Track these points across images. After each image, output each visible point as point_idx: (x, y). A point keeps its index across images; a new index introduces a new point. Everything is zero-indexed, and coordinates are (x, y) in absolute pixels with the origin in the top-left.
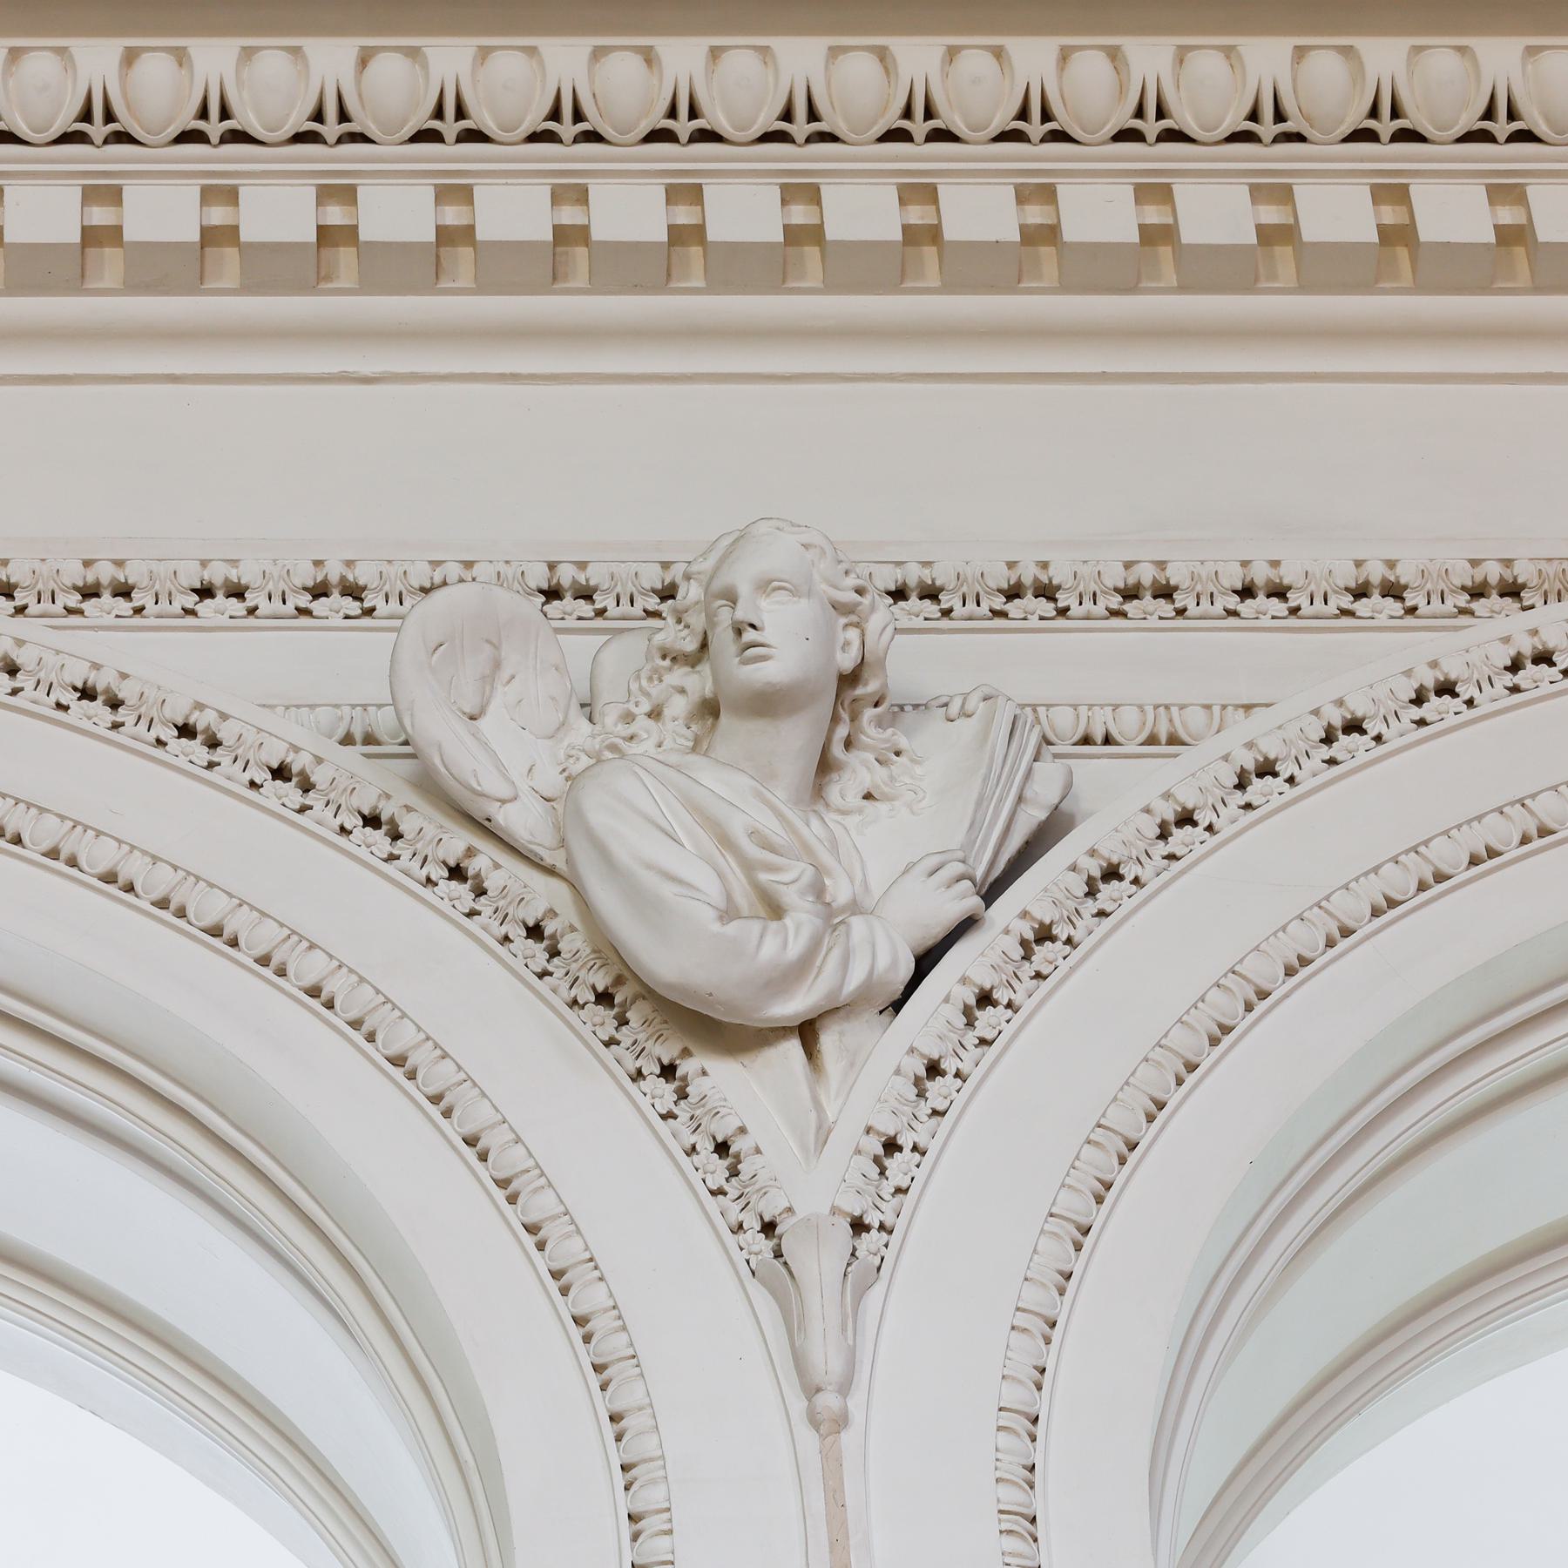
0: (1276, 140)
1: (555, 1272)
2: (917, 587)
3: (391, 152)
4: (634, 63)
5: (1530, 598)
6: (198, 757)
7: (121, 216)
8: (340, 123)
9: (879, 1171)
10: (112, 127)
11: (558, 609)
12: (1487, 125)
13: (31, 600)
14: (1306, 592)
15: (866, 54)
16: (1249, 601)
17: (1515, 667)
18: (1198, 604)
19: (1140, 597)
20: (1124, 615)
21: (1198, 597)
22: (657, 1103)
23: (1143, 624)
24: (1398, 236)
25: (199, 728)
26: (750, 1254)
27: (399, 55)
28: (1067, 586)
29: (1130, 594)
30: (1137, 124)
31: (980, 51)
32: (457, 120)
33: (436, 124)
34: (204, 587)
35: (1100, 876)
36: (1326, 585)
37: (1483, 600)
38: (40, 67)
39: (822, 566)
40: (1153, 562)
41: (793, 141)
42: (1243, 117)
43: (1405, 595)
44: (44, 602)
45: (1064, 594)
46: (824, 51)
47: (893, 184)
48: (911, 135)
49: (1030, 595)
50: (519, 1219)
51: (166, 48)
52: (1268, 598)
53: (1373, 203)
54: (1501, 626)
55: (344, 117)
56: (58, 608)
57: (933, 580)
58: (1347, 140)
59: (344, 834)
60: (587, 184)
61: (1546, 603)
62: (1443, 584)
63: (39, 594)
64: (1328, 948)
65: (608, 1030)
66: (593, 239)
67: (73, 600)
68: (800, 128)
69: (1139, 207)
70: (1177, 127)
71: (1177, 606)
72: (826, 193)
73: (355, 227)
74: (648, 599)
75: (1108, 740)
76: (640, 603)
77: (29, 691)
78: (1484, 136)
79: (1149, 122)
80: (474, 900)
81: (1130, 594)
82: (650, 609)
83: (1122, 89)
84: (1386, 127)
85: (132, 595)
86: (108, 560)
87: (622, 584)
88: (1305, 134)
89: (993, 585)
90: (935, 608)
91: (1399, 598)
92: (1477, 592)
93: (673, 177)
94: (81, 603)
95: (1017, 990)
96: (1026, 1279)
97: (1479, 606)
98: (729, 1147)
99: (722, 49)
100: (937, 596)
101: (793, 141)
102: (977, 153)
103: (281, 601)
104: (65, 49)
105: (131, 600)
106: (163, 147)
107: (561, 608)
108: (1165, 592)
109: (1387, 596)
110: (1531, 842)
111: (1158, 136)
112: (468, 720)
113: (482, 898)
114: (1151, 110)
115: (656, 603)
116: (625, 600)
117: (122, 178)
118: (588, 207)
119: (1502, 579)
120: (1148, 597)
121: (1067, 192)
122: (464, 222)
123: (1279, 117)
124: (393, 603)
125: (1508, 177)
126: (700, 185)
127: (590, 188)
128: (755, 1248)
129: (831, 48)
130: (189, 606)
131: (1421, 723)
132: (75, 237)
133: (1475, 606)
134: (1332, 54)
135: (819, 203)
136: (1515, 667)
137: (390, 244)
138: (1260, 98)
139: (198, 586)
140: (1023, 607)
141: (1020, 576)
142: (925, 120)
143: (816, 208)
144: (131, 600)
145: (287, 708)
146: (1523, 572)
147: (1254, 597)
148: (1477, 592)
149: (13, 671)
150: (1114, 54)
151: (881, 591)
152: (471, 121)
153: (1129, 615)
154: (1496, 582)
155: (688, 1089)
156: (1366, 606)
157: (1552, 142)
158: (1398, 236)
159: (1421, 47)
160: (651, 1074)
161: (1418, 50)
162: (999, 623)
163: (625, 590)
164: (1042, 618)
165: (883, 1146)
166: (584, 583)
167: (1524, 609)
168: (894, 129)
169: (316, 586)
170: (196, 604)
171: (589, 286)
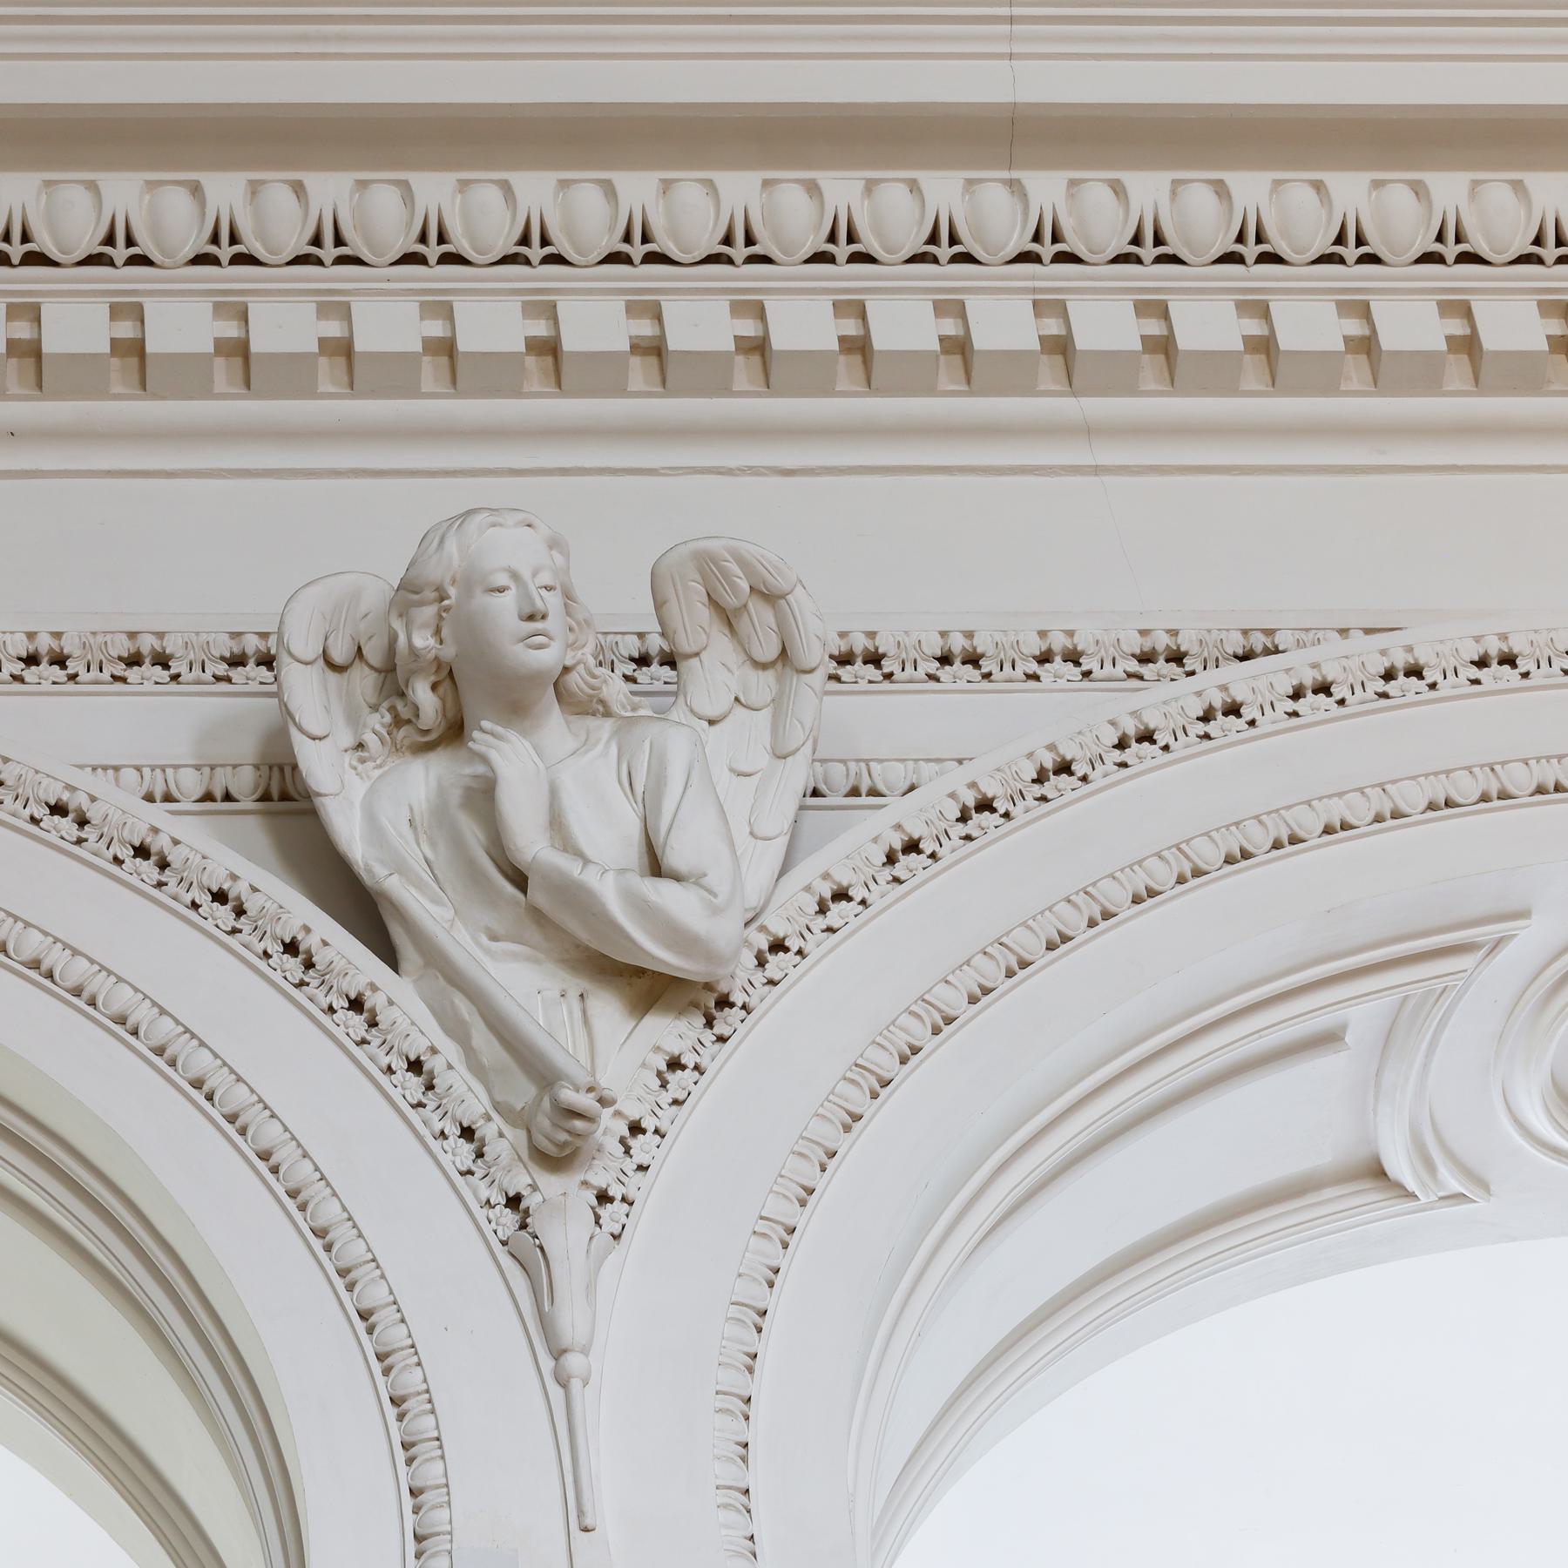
1: (342, 1270)
2: (48, 653)
5: (987, 666)
8: (335, 247)
11: (242, 674)
12: (1338, 249)
14: (1096, 658)
15: (1506, 184)
16: (947, 668)
18: (903, 670)
19: (1050, 660)
20: (229, 680)
21: (903, 663)
27: (1509, 186)
28: (1090, 652)
30: (1035, 247)
31: (1101, 183)
32: (848, 243)
33: (830, 248)
35: (830, 897)
36: (1217, 652)
39: (101, 640)
42: (1128, 241)
46: (554, 182)
50: (309, 1224)
51: (593, 180)
53: (1136, 315)
54: (1165, 690)
55: (339, 241)
56: (208, 676)
58: (807, 261)
60: (864, 300)
61: (1205, 669)
62: (1549, 650)
63: (1205, 660)
69: (1038, 320)
70: (1472, 250)
79: (942, 245)
87: (1105, 649)
88: (1380, 255)
91: (166, 667)
92: (1146, 658)
96: (740, 1275)
97: (1148, 670)
99: (263, 182)
102: (893, 273)
107: (245, 674)
109: (157, 664)
112: (727, 770)
113: (242, 919)
114: (1451, 236)
117: (750, 294)
119: (964, 648)
120: (1161, 661)
126: (451, 301)
127: (455, 305)
129: (1173, 181)
130: (629, 673)
134: (81, 188)
137: (84, 355)
138: (1544, 227)
139: (636, 655)
142: (642, 244)
145: (94, 769)
147: (38, 664)
148: (1146, 658)
150: (913, 186)
151: (626, 658)
152: (861, 245)
153: (233, 681)
161: (363, 184)
162: (119, 687)
164: (870, 682)
169: (130, 656)
170: (634, 670)
171: (1475, 389)
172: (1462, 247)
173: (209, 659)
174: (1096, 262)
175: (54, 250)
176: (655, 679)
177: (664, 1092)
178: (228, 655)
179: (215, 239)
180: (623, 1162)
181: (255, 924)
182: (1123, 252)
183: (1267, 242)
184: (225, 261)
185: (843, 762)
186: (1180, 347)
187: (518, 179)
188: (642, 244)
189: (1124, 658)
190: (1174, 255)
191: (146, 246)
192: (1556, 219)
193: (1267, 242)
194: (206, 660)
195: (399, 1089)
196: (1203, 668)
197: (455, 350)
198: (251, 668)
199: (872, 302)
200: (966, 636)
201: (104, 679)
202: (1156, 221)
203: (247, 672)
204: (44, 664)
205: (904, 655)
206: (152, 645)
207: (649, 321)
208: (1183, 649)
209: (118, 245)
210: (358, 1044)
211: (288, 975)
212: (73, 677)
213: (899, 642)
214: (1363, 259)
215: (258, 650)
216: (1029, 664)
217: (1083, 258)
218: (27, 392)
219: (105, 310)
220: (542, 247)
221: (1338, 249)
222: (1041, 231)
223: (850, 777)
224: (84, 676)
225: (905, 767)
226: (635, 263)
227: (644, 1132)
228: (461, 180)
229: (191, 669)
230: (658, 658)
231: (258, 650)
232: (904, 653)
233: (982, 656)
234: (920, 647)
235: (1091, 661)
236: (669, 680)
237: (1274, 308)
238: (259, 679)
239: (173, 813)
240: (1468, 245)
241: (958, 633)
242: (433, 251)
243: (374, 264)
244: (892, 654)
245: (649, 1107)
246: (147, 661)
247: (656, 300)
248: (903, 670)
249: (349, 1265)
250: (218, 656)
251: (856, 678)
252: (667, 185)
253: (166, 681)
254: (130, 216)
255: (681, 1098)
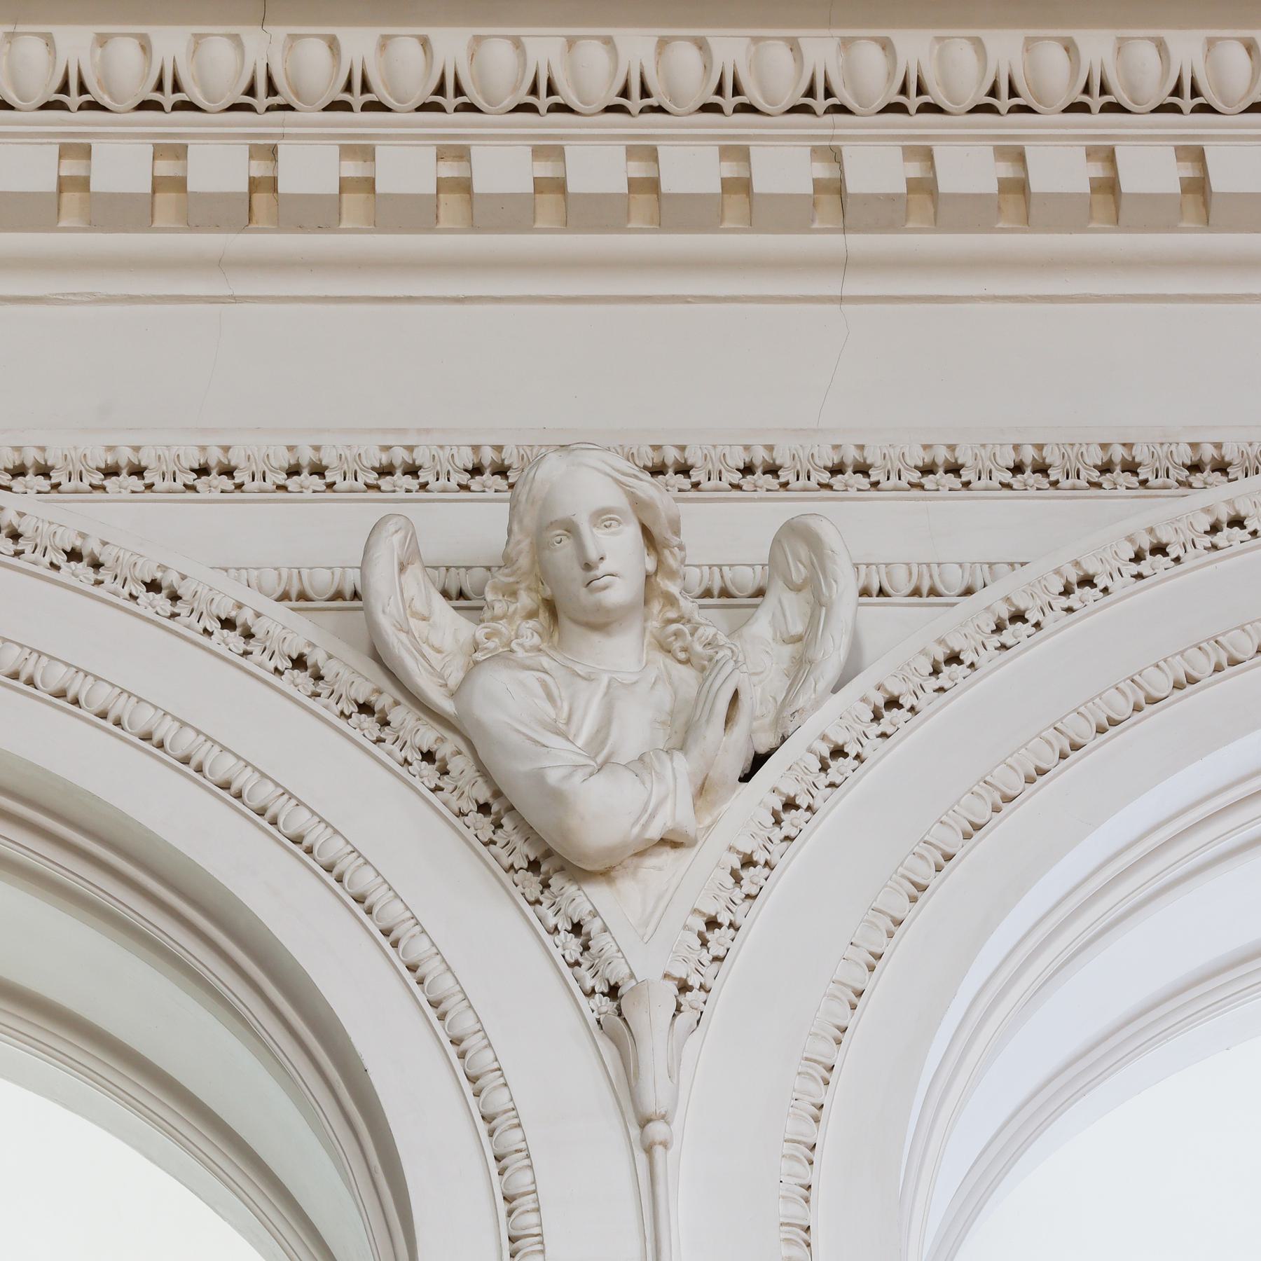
0: (268, 109)
3: (1051, 120)
4: (414, 49)
6: (161, 608)
7: (185, 168)
8: (268, 95)
9: (700, 943)
10: (461, 99)
13: (64, 480)
16: (749, 477)
17: (1215, 529)
18: (888, 479)
22: (527, 891)
23: (755, 495)
24: (924, 187)
25: (164, 584)
26: (600, 1014)
29: (385, 471)
33: (717, 99)
34: (1193, 464)
37: (931, 476)
38: (31, 49)
40: (1033, 445)
41: (814, 113)
43: (1138, 471)
44: (1072, 478)
45: (58, 472)
47: (1172, 146)
48: (351, 105)
49: (941, 472)
52: (492, 475)
56: (360, 485)
57: (46, 461)
59: (277, 674)
60: (749, 146)
64: (1061, 760)
65: (487, 834)
66: (475, 191)
67: (97, 478)
68: (635, 103)
71: (236, 482)
72: (755, 153)
73: (275, 180)
74: (369, 475)
75: (882, 592)
76: (816, 477)
77: (28, 554)
78: (344, 106)
80: (439, 778)
81: (385, 471)
82: (823, 481)
83: (890, 76)
84: (168, 99)
85: (145, 474)
86: (401, 446)
88: (664, 106)
89: (821, 464)
90: (141, 483)
91: (1135, 473)
93: (539, 140)
94: (103, 480)
95: (814, 796)
98: (582, 926)
99: (852, 40)
100: (1226, 470)
101: (814, 113)
102: (405, 120)
103: (79, 479)
104: (237, 35)
105: (143, 478)
106: (32, 111)
108: (955, 469)
110: (1224, 670)
111: (1010, 109)
114: (913, 88)
115: (283, 479)
116: (803, 476)
117: (472, 140)
118: (750, 164)
121: (572, 152)
122: (270, 174)
123: (645, 93)
124: (443, 480)
125: (171, 138)
128: (604, 1009)
130: (735, 482)
131: (1139, 576)
132: (52, 187)
133: (924, 480)
135: (656, 160)
136: (1215, 529)
140: (753, 482)
141: (1111, 456)
142: (548, 96)
143: (561, 164)
144: (143, 478)
146: (1230, 454)
147: (753, 474)
148: (1195, 468)
149: (15, 536)
150: (517, 43)
153: (834, 488)
154: (489, 463)
155: (550, 882)
156: (1199, 480)
157: (1136, 111)
158: (924, 187)
159: (296, 35)
160: (521, 868)
161: (293, 37)
163: (1073, 464)
165: (706, 924)
166: (43, 463)
167: (1230, 481)
168: (1076, 103)
169: (290, 467)
172: (369, 97)
173: (361, 469)
174: (1140, 111)
175: (762, 101)
176: (398, 487)
177: (738, 889)
178: (920, 464)
179: (904, 90)
180: (701, 953)
181: (332, 688)
182: (1076, 101)
183: (87, 92)
184: (912, 109)
185: (751, 565)
186: (1214, 189)
187: (1173, 37)
188: (548, 96)
189: (1175, 468)
190: (1026, 106)
191: (1209, 96)
192: (722, 73)
193: (87, 92)
194: (902, 469)
195: (560, 949)
196: (435, 479)
197: (750, 189)
198: (849, 476)
199: (663, 147)
200: (1215, 447)
201: (268, 488)
202: (1193, 79)
203: (26, 482)
204: (487, 474)
205: (71, 468)
206: (129, 459)
207: (1190, 164)
208: (417, 463)
209: (818, 98)
210: (486, 844)
211: (366, 732)
212: (785, 485)
213: (885, 454)
214: (179, 106)
215: (404, 462)
216: (913, 474)
217: (575, 109)
218: (1193, 226)
219: (1082, 152)
220: (826, 99)
221: (808, 101)
222: (723, 85)
223: (860, 580)
224: (794, 484)
225: (439, 573)
226: (166, 111)
227: (720, 926)
228: (196, 34)
229: (164, 479)
230: (127, 469)
231: (404, 462)
232: (346, 465)
233: (1230, 464)
234: (995, 459)
235: (243, 475)
236: (42, 490)
237: (846, 152)
238: (856, 486)
239: (293, 609)
240: (835, 98)
241: (1208, 445)
242: (1096, 101)
243: (675, 114)
244: (1057, 465)
245: (724, 904)
246: (1208, 468)
247: (927, 146)
248: (888, 479)
249: (478, 1073)
250: (95, 467)
251: (938, 485)
252: (571, 42)
253: (866, 488)
254: (82, 68)
255: (754, 893)
